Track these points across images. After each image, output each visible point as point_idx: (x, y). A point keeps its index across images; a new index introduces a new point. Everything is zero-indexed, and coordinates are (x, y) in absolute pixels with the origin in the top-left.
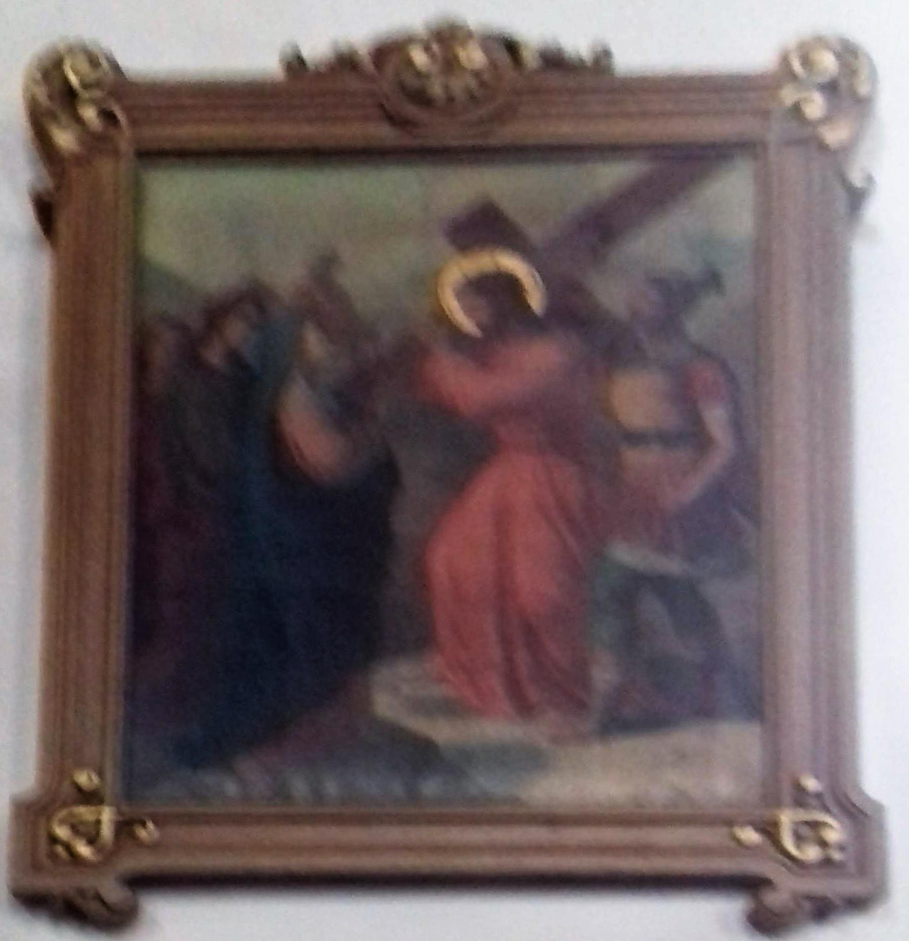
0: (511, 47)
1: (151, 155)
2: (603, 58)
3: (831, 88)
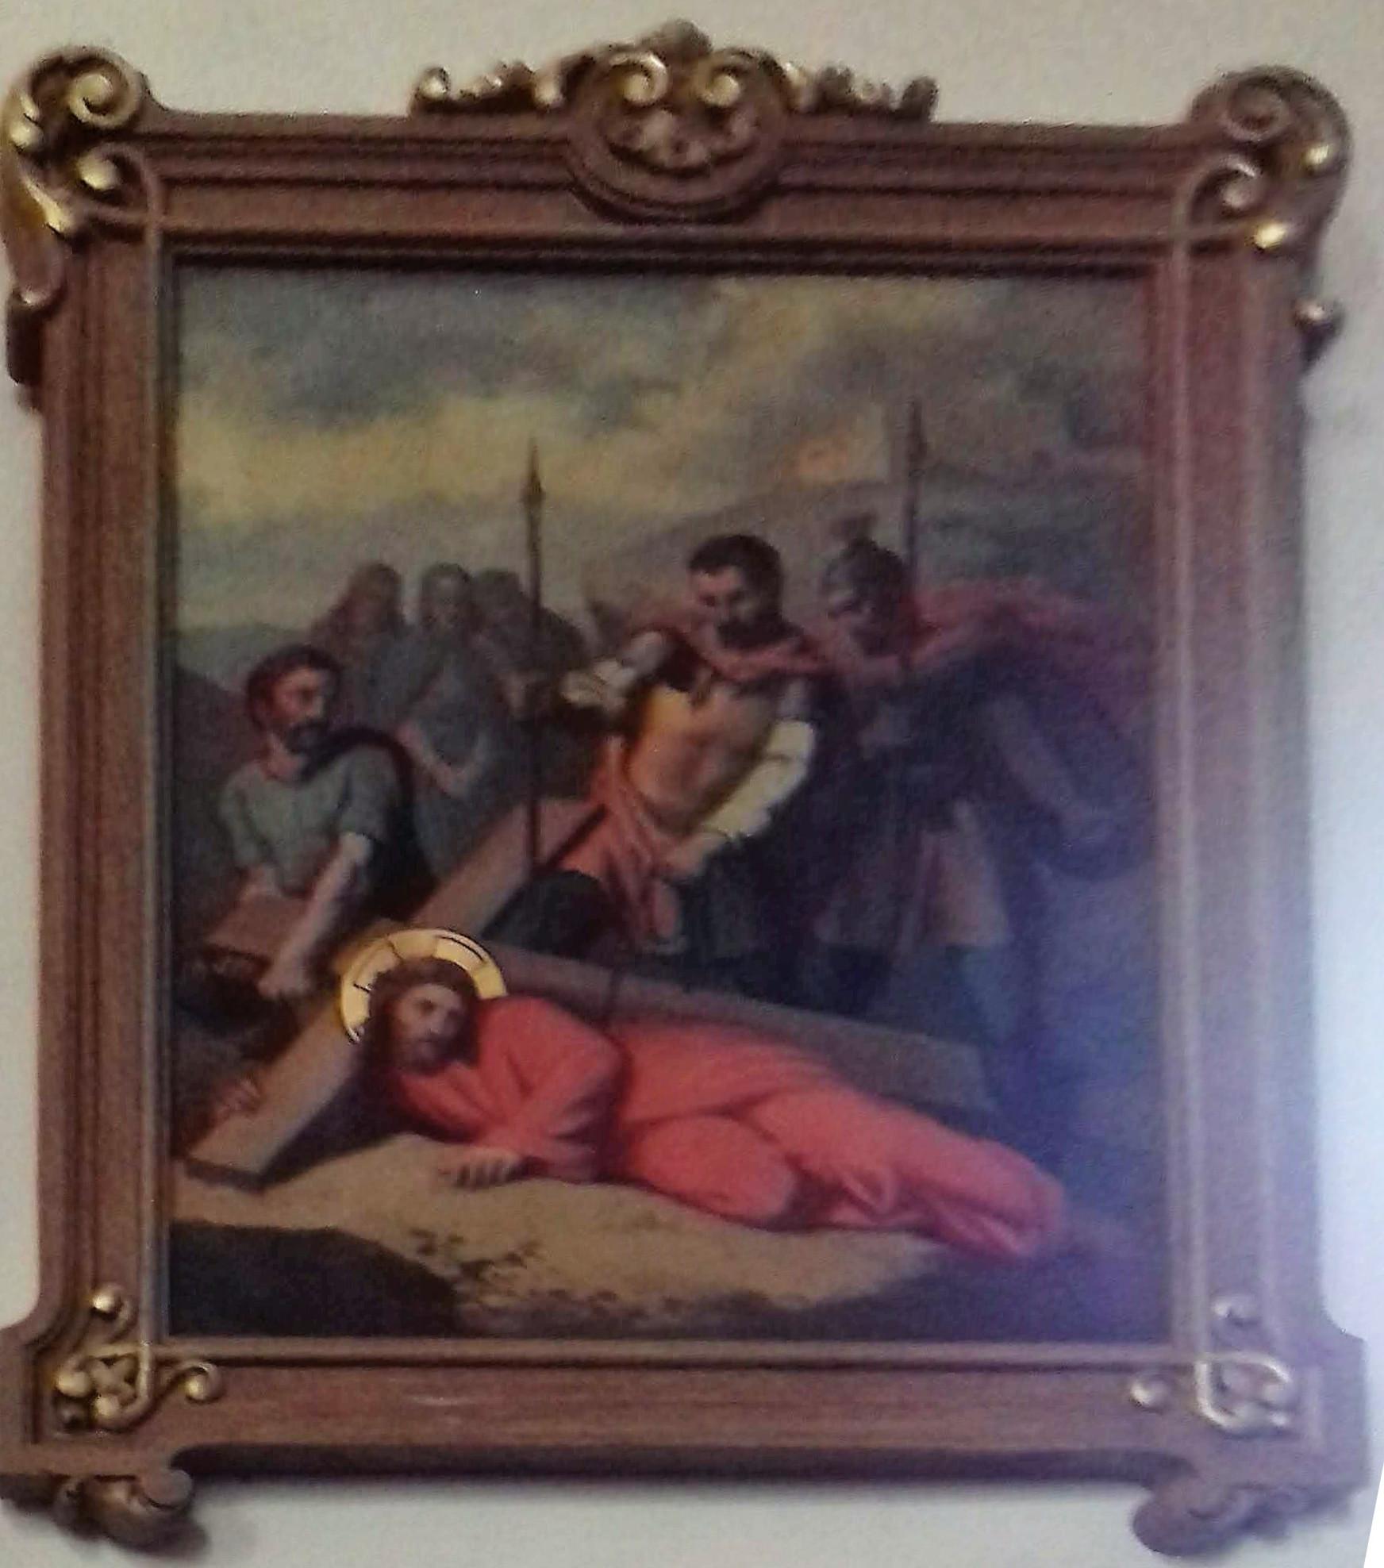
1: (197, 256)
2: (921, 97)
3: (1265, 156)
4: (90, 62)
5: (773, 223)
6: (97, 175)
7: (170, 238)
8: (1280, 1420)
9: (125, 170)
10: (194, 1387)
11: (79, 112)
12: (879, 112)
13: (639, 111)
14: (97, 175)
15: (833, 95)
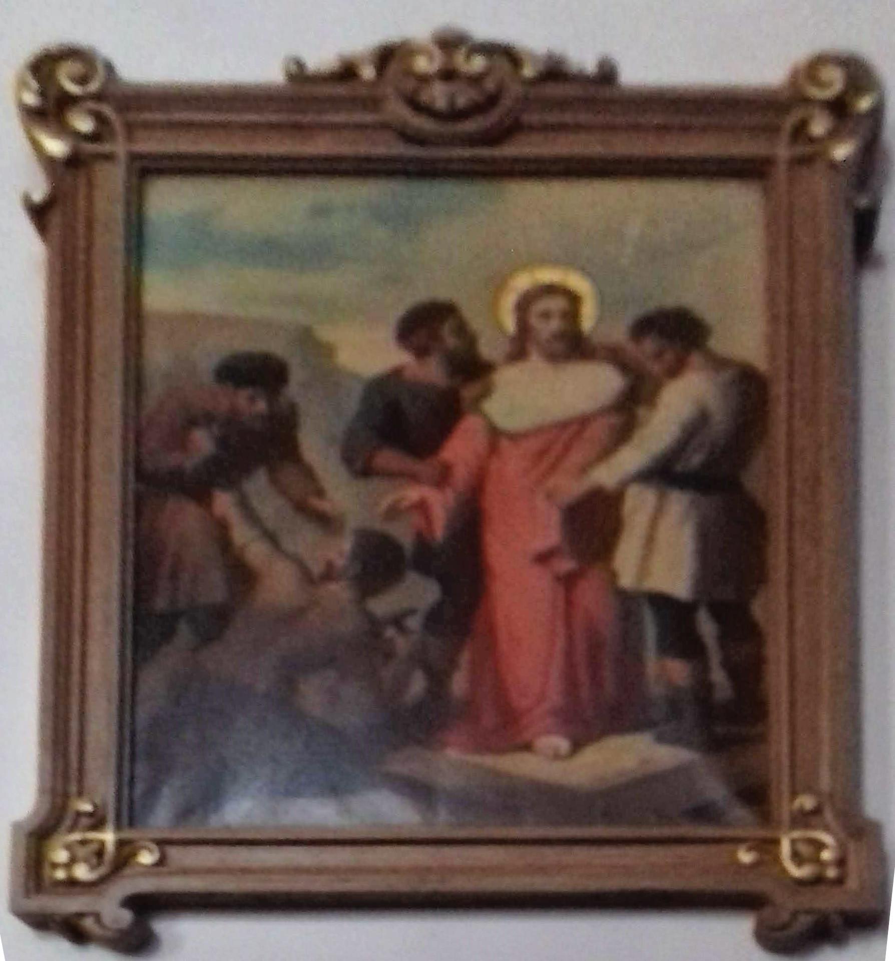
0: (507, 55)
1: (146, 169)
2: (607, 74)
4: (72, 53)
5: (509, 150)
6: (84, 124)
7: (134, 157)
8: (831, 873)
9: (99, 118)
10: (146, 858)
11: (59, 84)
12: (580, 79)
13: (424, 79)
14: (84, 124)
15: (555, 71)
